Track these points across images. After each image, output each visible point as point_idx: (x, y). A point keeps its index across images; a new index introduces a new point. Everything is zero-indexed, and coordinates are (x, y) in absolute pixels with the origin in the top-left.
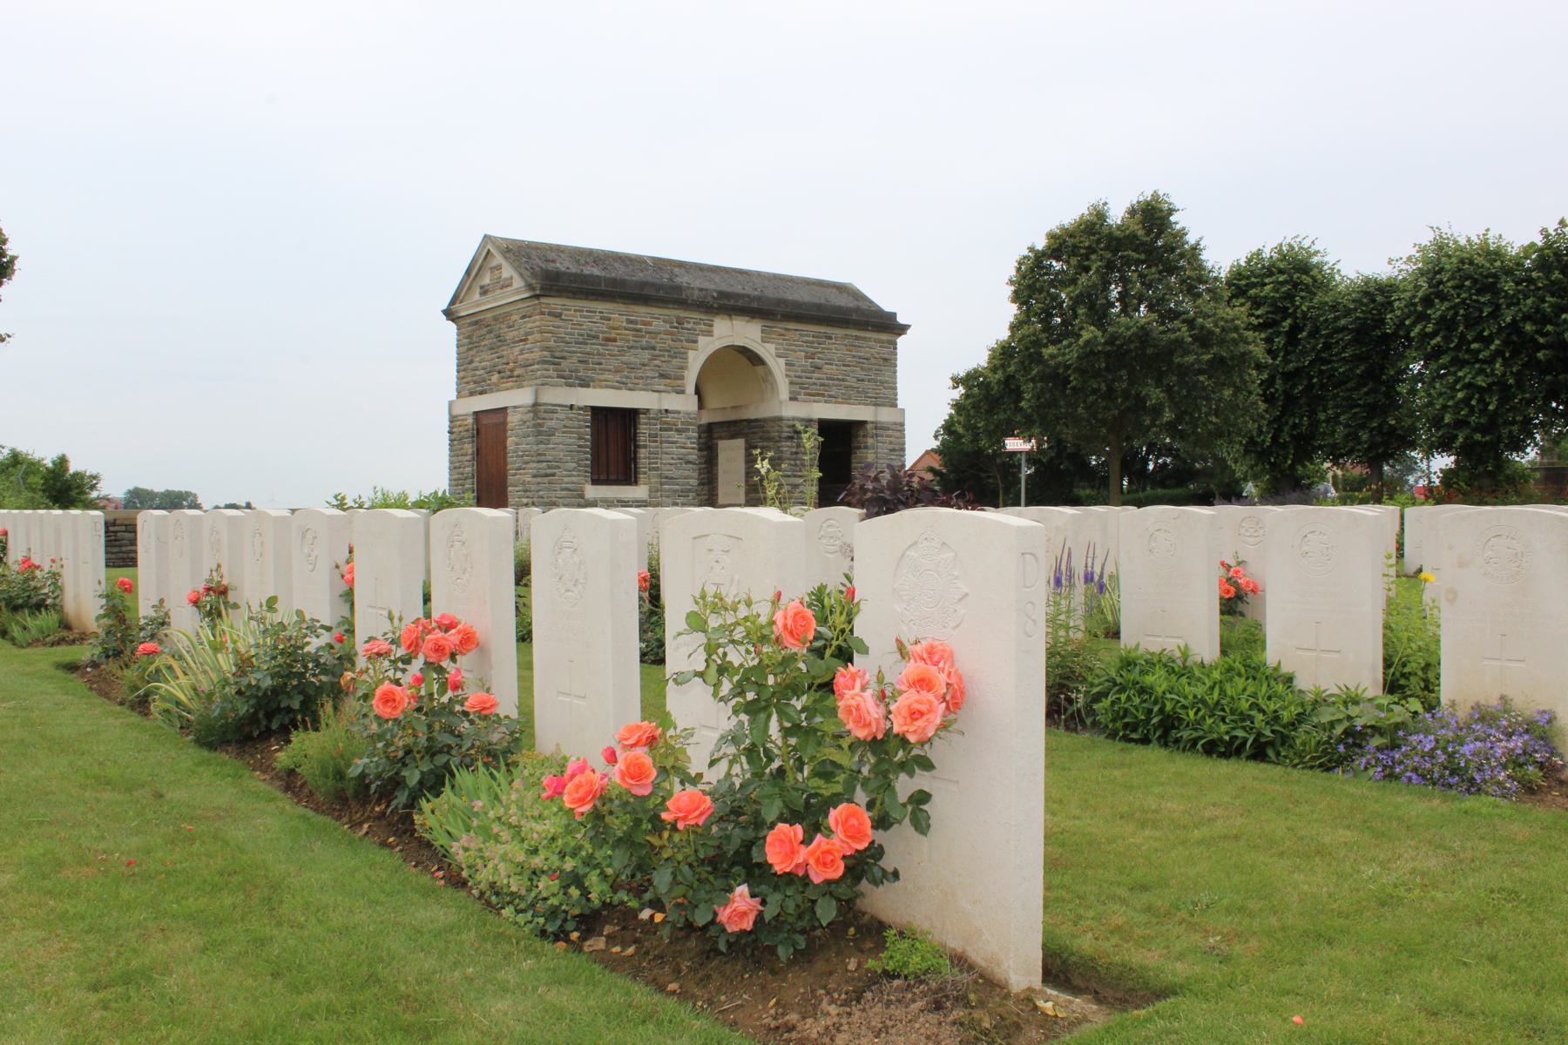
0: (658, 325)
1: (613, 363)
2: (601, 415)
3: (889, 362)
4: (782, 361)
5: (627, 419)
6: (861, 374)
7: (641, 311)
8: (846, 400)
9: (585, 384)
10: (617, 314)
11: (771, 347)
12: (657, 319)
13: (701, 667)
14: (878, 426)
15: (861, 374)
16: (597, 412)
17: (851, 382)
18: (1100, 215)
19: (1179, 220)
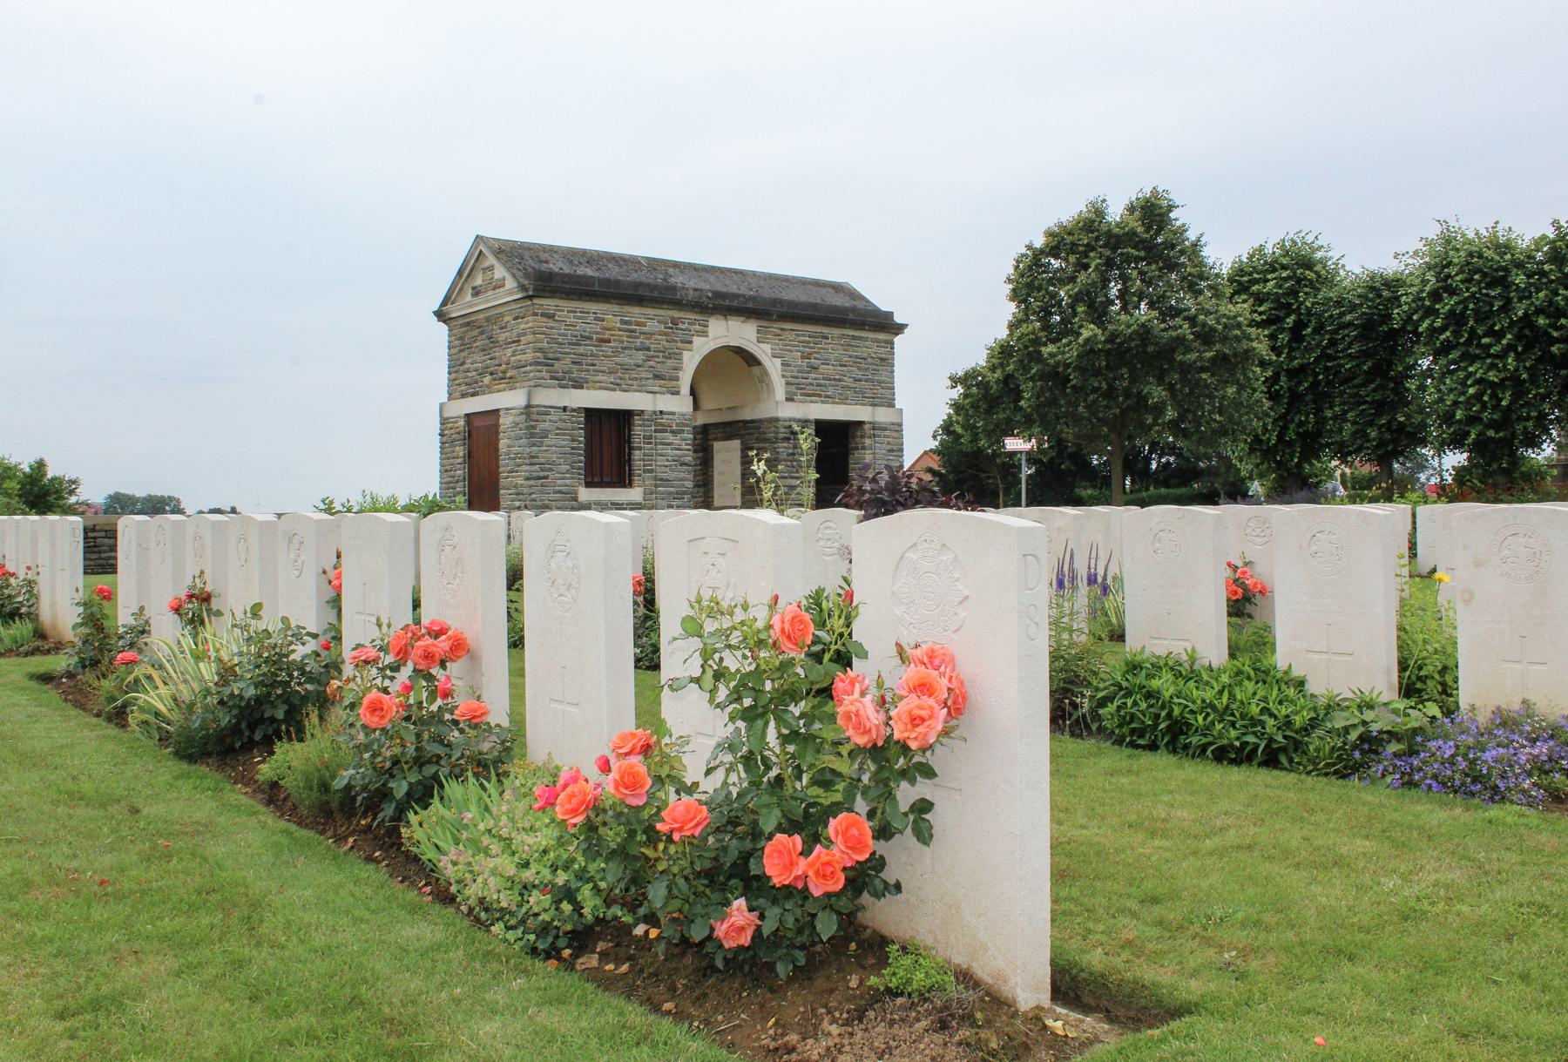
0: (652, 326)
1: (608, 364)
3: (887, 362)
4: (778, 362)
5: (623, 419)
6: (858, 374)
8: (843, 401)
9: (578, 385)
10: (611, 314)
11: (767, 348)
12: (651, 319)
14: (875, 426)
16: (592, 414)
17: (848, 381)
18: (1099, 213)
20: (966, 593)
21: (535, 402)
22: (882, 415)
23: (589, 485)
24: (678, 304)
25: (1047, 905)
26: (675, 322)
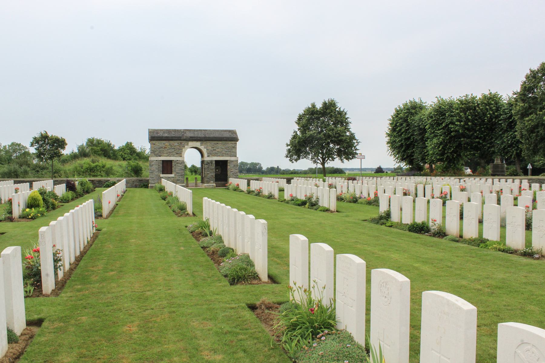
0: (176, 144)
1: (166, 152)
2: (163, 162)
3: (235, 147)
4: (205, 149)
5: (225, 163)
6: (226, 150)
7: (172, 142)
8: (223, 156)
9: (160, 156)
10: (167, 143)
11: (203, 147)
12: (176, 143)
13: (28, 184)
14: (232, 161)
15: (226, 150)
16: (163, 161)
17: (224, 152)
18: (314, 106)
19: (50, 134)
20: (397, 195)
21: (326, 165)
22: (233, 159)
23: (163, 173)
24: (181, 140)
25: (409, 290)
26: (181, 143)
